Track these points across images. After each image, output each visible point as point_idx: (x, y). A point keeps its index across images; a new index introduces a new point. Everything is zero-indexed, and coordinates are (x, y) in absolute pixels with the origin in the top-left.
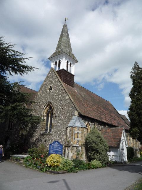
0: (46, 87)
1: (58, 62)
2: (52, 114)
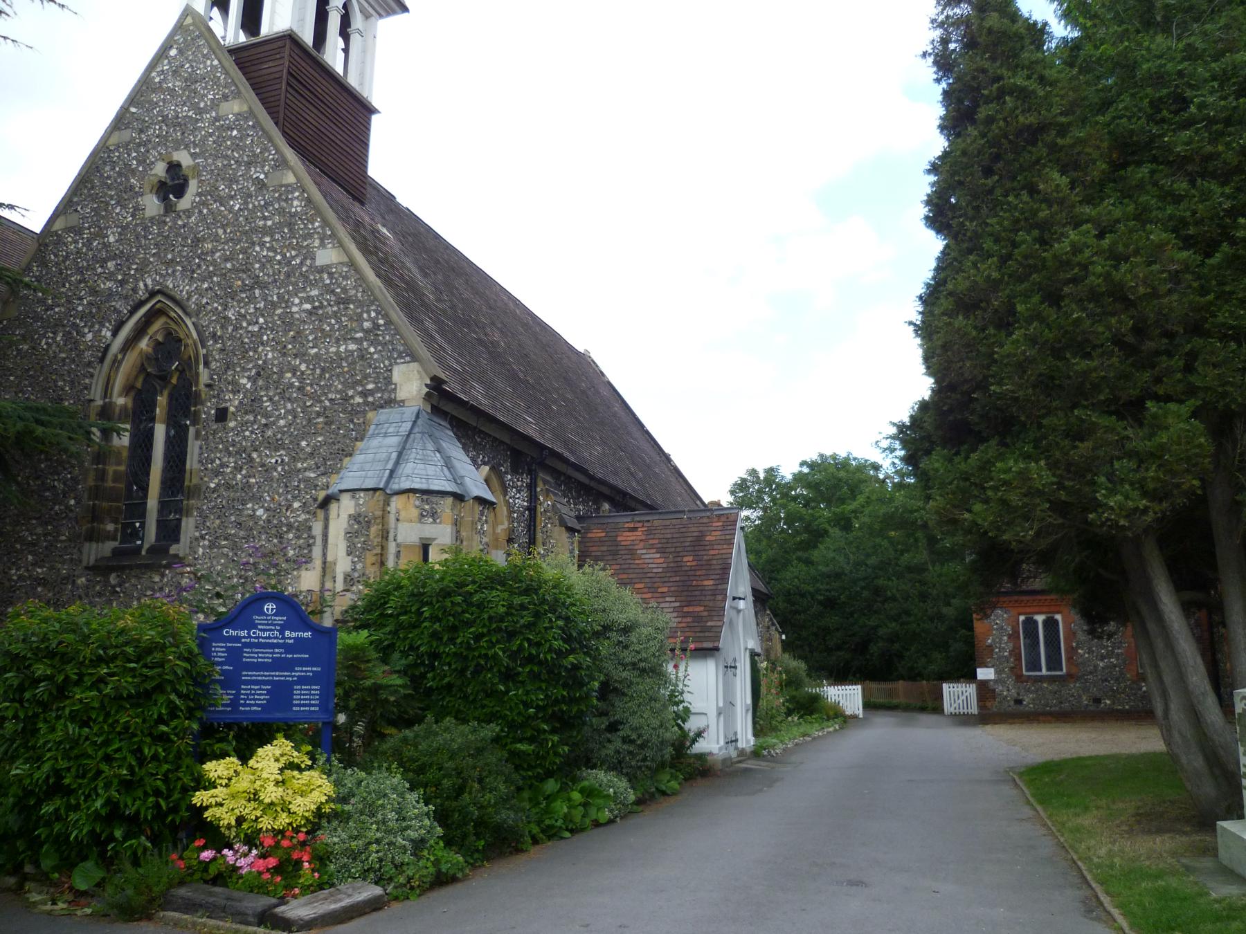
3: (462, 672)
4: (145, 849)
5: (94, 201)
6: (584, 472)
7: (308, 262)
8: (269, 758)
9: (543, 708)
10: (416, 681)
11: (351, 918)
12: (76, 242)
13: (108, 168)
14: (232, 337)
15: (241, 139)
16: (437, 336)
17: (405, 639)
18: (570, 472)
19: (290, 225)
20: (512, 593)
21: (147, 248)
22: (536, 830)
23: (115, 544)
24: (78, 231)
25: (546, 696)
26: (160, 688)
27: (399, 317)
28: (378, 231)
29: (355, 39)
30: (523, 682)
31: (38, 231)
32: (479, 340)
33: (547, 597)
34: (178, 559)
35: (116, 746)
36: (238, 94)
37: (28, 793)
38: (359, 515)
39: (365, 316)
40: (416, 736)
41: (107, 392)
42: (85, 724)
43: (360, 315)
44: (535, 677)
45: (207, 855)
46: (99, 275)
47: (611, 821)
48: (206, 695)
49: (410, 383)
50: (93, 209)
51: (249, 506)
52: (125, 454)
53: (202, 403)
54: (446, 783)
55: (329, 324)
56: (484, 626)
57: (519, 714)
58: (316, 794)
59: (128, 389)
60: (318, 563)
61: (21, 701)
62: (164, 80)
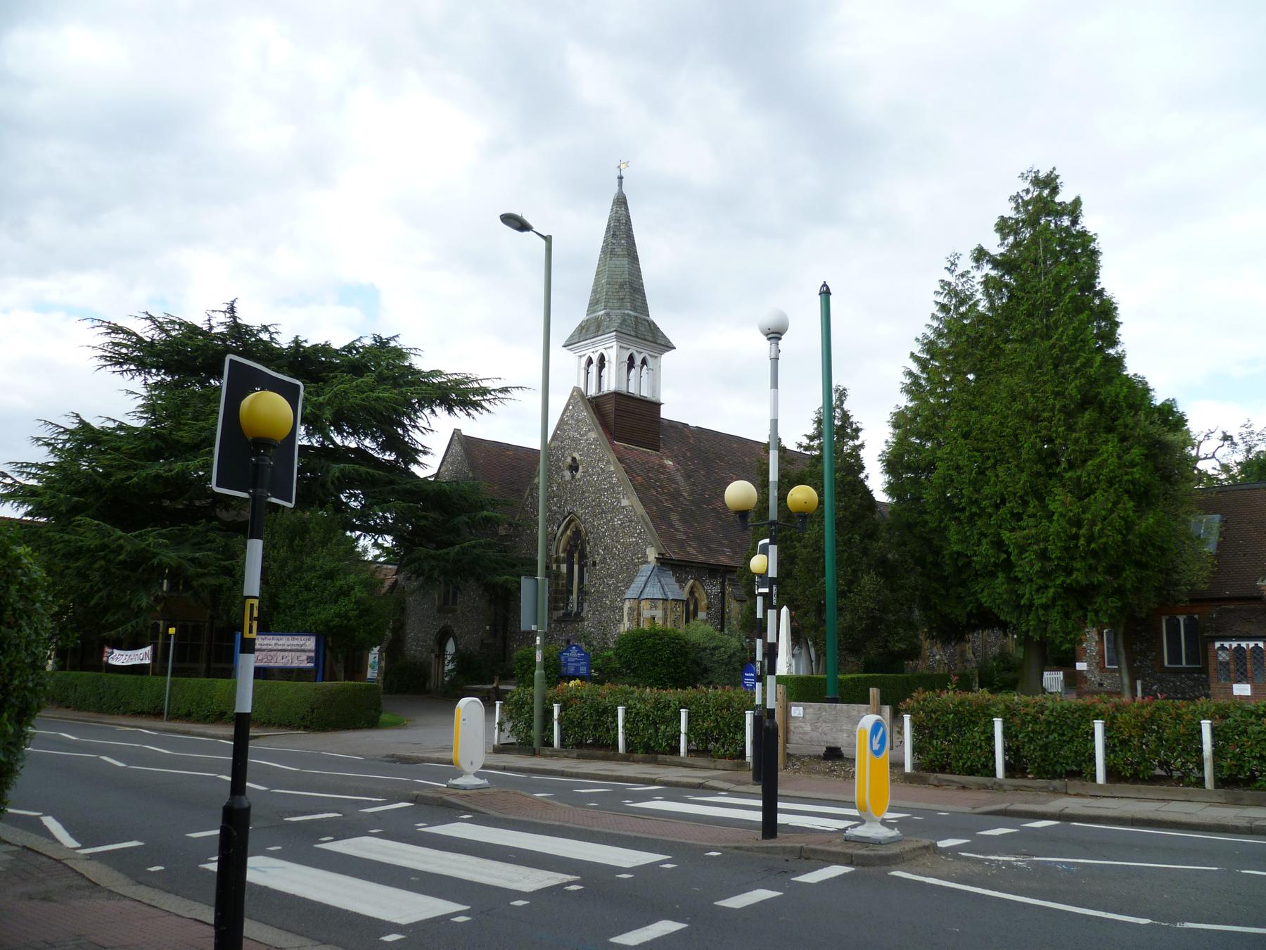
0: (558, 460)
1: (595, 358)
2: (583, 556)
49: (652, 554)
59: (564, 550)
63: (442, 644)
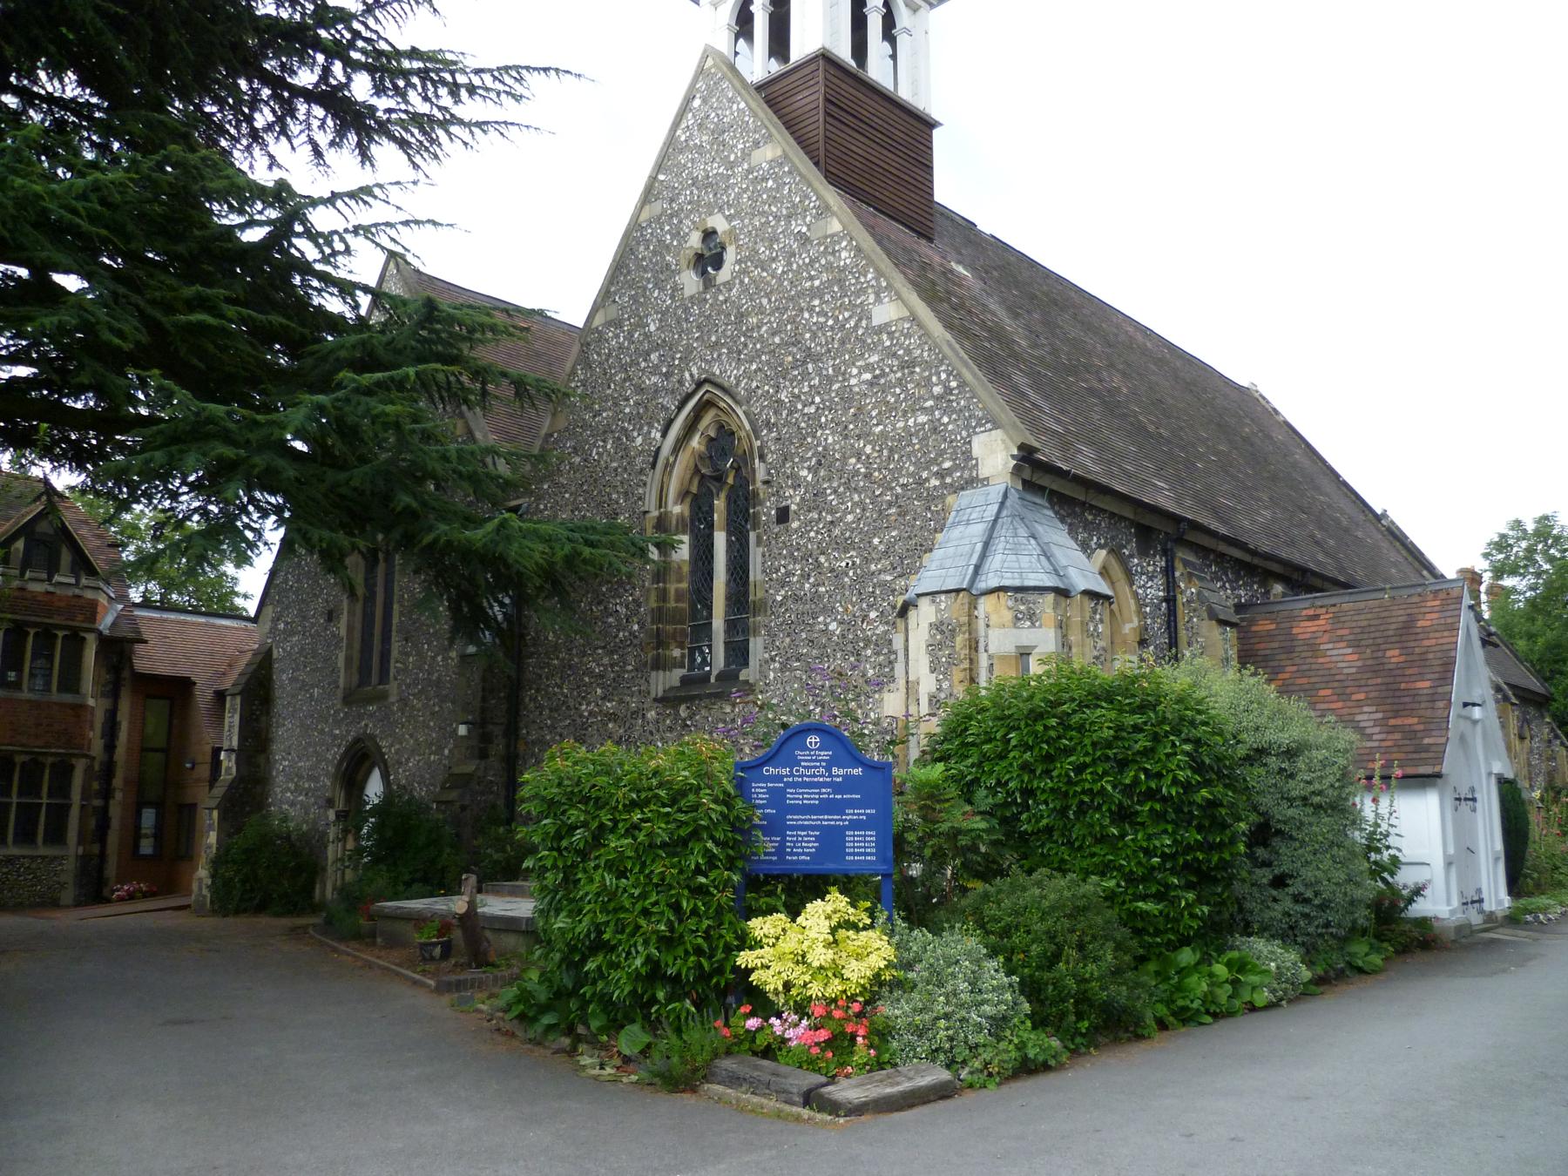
3: (1063, 812)
4: (688, 1012)
5: (630, 287)
6: (1242, 546)
7: (864, 323)
8: (818, 915)
9: (1173, 856)
10: (1008, 823)
11: (911, 1106)
12: (617, 336)
13: (642, 248)
14: (787, 423)
15: (777, 190)
16: (1030, 393)
17: (992, 772)
18: (1223, 548)
19: (841, 282)
20: (1121, 711)
21: (689, 331)
22: (1162, 1010)
23: (684, 671)
24: (617, 323)
25: (1175, 841)
26: (695, 834)
27: (974, 375)
28: (952, 271)
29: (902, 40)
30: (1142, 824)
31: (581, 325)
32: (1091, 391)
33: (1169, 715)
34: (748, 688)
35: (653, 899)
36: (769, 138)
37: (573, 950)
38: (942, 623)
39: (934, 379)
40: (999, 891)
41: (661, 501)
42: (622, 874)
43: (929, 378)
44: (1159, 817)
45: (753, 1023)
46: (643, 370)
47: (1270, 1006)
48: (748, 842)
49: (994, 455)
50: (631, 297)
51: (821, 619)
52: (686, 569)
53: (761, 503)
54: (1035, 949)
55: (894, 394)
56: (1087, 754)
57: (1139, 863)
58: (873, 957)
59: (683, 495)
60: (901, 682)
61: (559, 850)
62: (690, 137)
63: (352, 779)
